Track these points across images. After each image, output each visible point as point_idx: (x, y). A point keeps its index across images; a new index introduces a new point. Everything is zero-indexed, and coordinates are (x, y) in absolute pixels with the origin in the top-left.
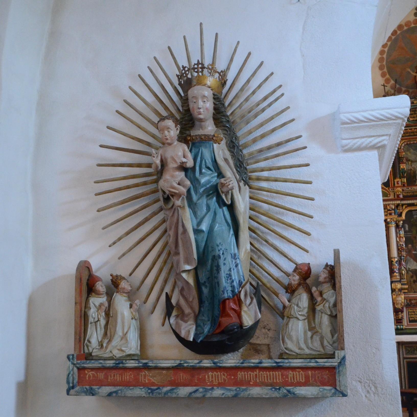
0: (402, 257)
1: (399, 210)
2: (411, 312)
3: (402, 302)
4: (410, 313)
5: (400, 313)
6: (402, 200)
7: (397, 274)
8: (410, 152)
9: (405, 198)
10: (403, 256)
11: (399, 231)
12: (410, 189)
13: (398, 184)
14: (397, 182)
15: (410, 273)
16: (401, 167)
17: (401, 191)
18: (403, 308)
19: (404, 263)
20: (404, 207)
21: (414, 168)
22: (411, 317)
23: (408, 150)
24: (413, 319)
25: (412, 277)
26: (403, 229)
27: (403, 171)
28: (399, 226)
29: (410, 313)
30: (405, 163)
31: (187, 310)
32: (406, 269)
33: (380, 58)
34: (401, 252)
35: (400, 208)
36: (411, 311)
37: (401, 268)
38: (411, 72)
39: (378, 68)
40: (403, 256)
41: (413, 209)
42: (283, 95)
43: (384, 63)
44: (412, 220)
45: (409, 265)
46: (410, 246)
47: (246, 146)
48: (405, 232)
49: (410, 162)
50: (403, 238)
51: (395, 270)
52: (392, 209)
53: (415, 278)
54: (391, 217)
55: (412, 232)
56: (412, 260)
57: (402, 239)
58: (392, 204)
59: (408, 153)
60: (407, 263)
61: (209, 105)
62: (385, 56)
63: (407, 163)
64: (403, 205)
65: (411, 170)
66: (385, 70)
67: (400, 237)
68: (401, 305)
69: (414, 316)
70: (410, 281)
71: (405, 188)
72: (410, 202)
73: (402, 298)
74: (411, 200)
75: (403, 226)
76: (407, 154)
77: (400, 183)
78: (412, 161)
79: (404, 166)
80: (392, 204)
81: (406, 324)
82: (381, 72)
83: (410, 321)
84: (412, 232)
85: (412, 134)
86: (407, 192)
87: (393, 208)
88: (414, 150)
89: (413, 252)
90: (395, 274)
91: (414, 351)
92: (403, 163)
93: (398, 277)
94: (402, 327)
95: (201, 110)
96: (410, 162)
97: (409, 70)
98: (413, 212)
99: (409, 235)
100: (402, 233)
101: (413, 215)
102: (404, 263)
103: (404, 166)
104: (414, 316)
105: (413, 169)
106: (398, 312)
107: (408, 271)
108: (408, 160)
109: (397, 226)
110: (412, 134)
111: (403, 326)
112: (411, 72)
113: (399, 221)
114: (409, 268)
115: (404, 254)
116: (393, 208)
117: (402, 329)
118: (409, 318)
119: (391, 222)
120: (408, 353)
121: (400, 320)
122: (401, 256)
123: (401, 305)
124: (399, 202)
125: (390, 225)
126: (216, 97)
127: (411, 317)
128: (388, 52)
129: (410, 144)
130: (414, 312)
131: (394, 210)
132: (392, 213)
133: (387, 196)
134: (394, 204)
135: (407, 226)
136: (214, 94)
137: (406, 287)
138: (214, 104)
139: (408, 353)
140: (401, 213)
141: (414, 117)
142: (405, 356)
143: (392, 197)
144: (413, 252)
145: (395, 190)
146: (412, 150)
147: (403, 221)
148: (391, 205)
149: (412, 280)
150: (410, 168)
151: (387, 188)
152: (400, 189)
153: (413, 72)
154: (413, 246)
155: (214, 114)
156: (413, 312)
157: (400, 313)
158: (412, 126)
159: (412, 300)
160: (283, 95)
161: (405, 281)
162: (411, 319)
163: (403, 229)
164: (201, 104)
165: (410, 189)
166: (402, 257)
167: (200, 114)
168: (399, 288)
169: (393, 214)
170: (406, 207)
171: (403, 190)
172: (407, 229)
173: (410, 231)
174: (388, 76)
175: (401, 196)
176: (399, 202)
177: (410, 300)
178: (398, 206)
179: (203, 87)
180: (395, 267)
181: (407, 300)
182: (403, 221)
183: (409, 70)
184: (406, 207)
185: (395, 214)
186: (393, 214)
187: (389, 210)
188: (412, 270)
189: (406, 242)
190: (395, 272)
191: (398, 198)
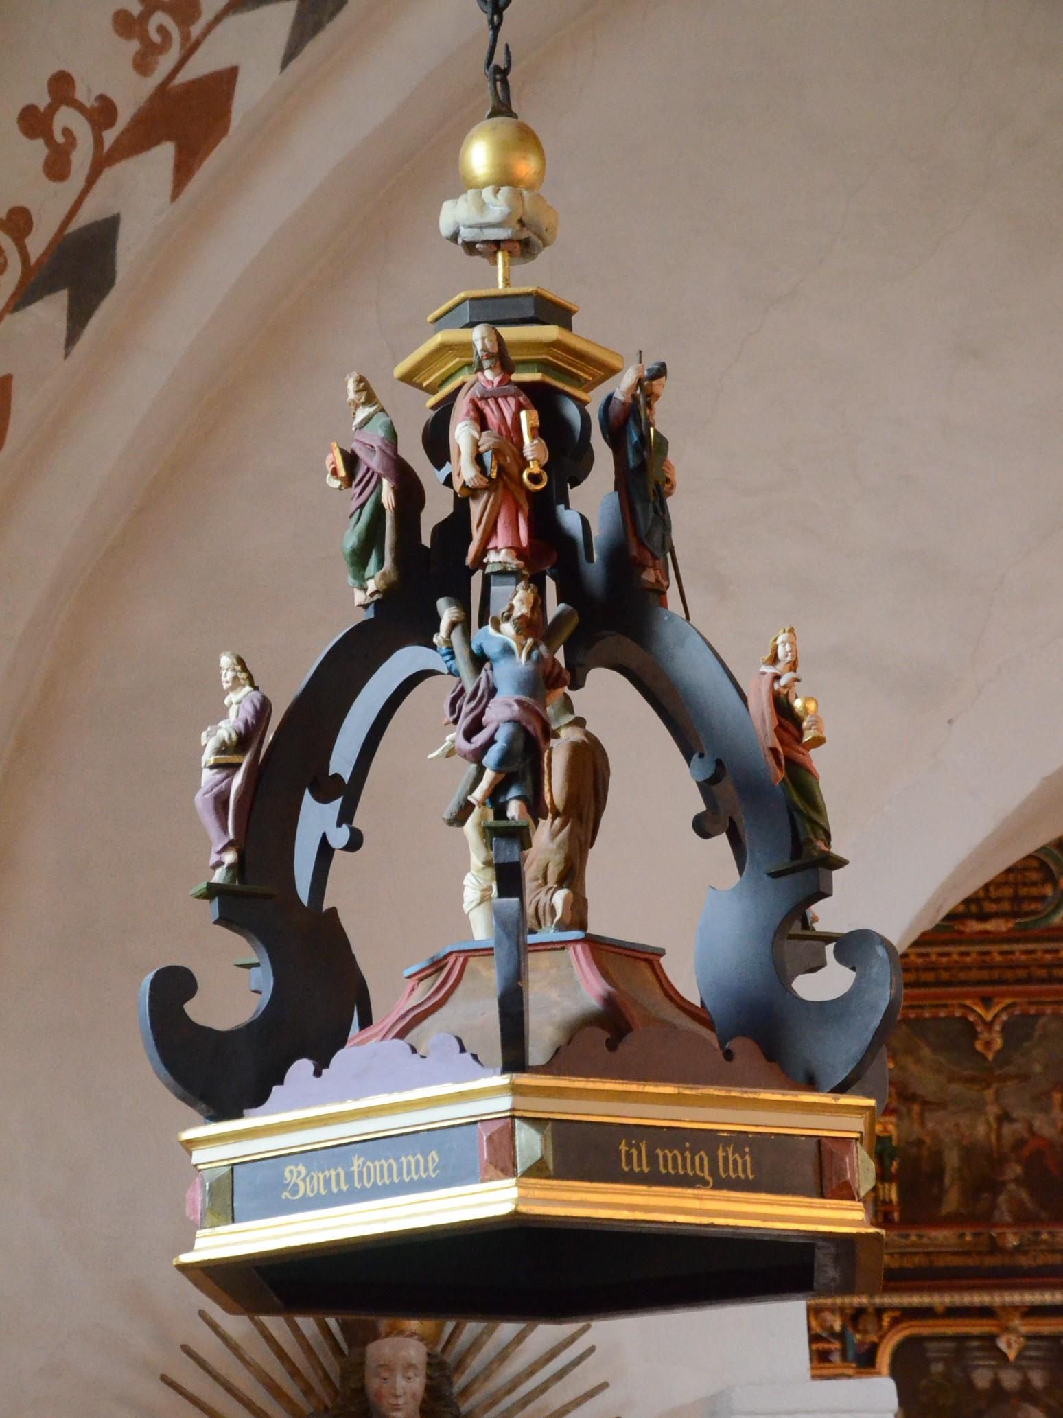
1: (865, 1332)
8: (918, 1061)
12: (913, 1238)
20: (886, 1322)
31: (166, 63)
35: (868, 1322)
42: (592, 1350)
44: (924, 1383)
47: (466, 1392)
49: (916, 1108)
52: (833, 1334)
58: (832, 1310)
59: (909, 1062)
61: (417, 1384)
63: (904, 1109)
64: (880, 1311)
65: (920, 1143)
72: (916, 1300)
74: (919, 1290)
76: (901, 1068)
78: (925, 1104)
79: (891, 1128)
80: (832, 1310)
85: (930, 977)
86: (902, 1255)
87: (837, 1327)
88: (934, 1049)
95: (401, 1401)
98: (931, 1345)
103: (891, 1128)
105: (928, 1140)
110: (930, 977)
116: (837, 1327)
126: (434, 1361)
129: (919, 1019)
131: (841, 1337)
136: (429, 1355)
138: (429, 1377)
146: (926, 1052)
150: (916, 1131)
155: (424, 1401)
160: (592, 1350)
164: (400, 1383)
165: (913, 1238)
167: (398, 1410)
169: (836, 1358)
178: (855, 1317)
179: (408, 1340)
184: (895, 1322)
185: (844, 1357)
186: (836, 1358)
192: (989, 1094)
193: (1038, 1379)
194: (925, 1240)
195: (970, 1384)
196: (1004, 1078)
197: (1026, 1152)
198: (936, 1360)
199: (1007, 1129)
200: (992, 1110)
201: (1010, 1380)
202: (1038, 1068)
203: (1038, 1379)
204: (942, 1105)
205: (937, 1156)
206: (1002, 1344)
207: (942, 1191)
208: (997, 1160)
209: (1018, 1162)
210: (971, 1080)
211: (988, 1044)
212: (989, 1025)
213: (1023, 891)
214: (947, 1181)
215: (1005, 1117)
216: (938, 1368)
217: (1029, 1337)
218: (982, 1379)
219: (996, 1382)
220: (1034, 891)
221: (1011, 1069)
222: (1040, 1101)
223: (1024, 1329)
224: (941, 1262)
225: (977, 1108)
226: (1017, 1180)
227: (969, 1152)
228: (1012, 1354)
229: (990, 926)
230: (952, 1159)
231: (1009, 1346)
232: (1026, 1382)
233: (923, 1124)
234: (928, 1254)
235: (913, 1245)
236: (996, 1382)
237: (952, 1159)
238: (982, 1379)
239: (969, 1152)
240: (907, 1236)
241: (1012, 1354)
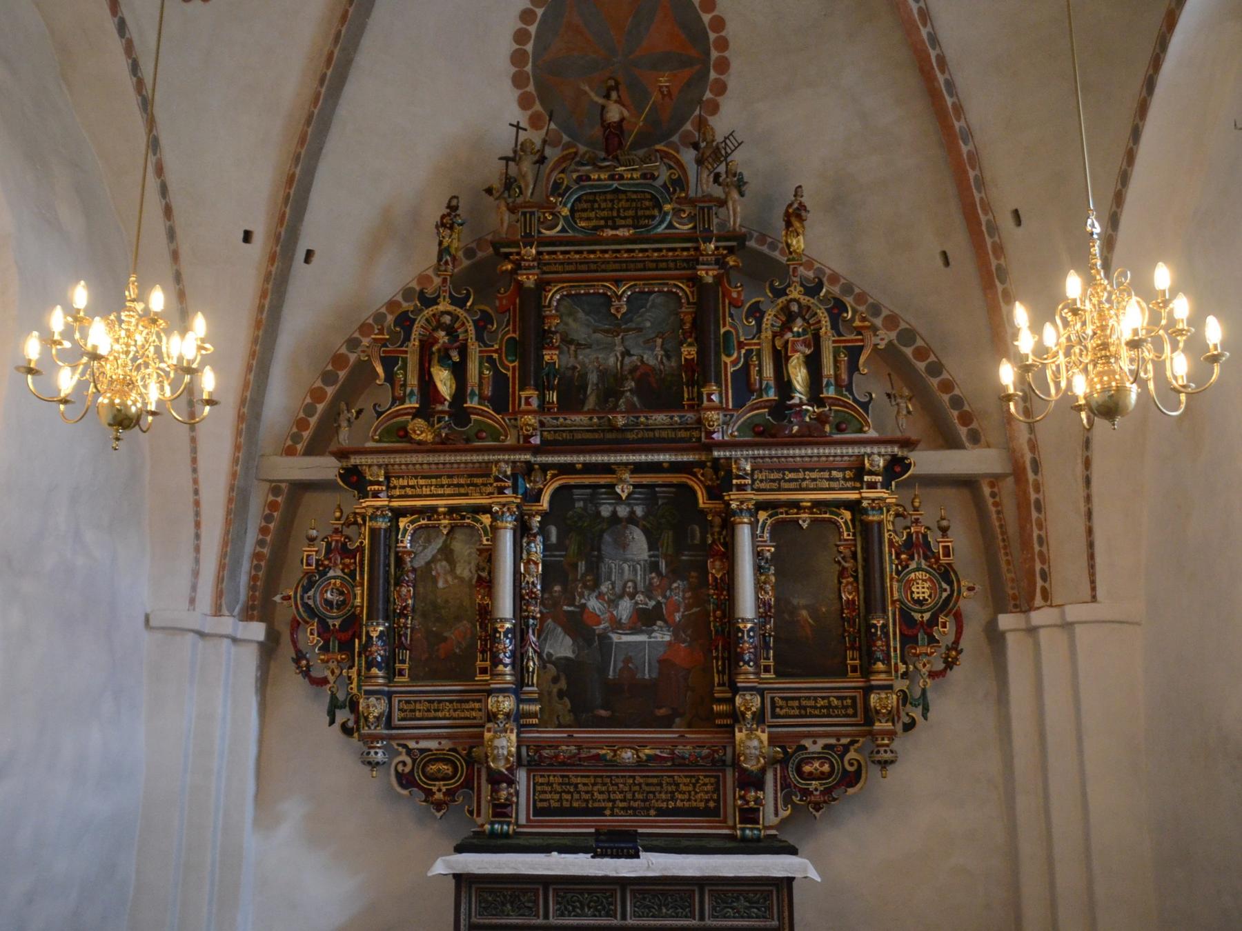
0: (531, 621)
1: (535, 482)
2: (542, 784)
3: (509, 752)
4: (539, 788)
5: (505, 785)
6: (536, 451)
7: (508, 670)
9: (547, 447)
10: (534, 618)
11: (528, 544)
12: (561, 420)
13: (528, 403)
14: (527, 398)
15: (552, 669)
16: (547, 358)
17: (537, 425)
18: (763, 771)
19: (533, 639)
21: (583, 364)
22: (541, 800)
23: (571, 314)
24: (545, 804)
25: (555, 680)
26: (539, 538)
27: (552, 370)
28: (531, 529)
29: (539, 788)
30: (558, 348)
32: (540, 655)
33: (516, 51)
34: (528, 604)
35: (537, 476)
36: (541, 780)
37: (527, 651)
38: (592, 94)
39: (510, 82)
40: (534, 618)
41: (572, 482)
43: (529, 68)
45: (551, 646)
46: (557, 588)
48: (545, 549)
49: (573, 348)
50: (536, 564)
51: (501, 656)
53: (563, 684)
54: (503, 500)
55: (566, 549)
56: (560, 629)
57: (532, 566)
58: (507, 462)
59: (570, 321)
60: (545, 639)
62: (529, 47)
64: (545, 468)
65: (574, 368)
66: (531, 88)
67: (529, 561)
68: (507, 760)
69: (548, 796)
70: (550, 693)
71: (547, 419)
73: (509, 740)
74: (565, 453)
75: (543, 530)
76: (566, 324)
77: (535, 403)
78: (579, 345)
79: (555, 357)
80: (507, 462)
81: (522, 820)
82: (517, 93)
83: (538, 812)
84: (566, 549)
85: (584, 267)
87: (509, 473)
88: (587, 314)
89: (565, 608)
90: (501, 667)
91: (504, 904)
92: (553, 348)
93: (508, 678)
94: (505, 827)
96: (573, 348)
97: (587, 88)
99: (558, 556)
100: (537, 548)
101: (573, 501)
102: (533, 639)
103: (555, 357)
104: (548, 796)
106: (499, 783)
107: (545, 661)
108: (567, 341)
109: (523, 530)
111: (509, 824)
112: (592, 94)
113: (532, 516)
114: (549, 655)
115: (535, 610)
117: (506, 835)
118: (535, 801)
119: (503, 513)
120: (485, 909)
121: (504, 806)
122: (528, 617)
123: (507, 760)
124: (528, 457)
125: (499, 524)
127: (541, 800)
128: (537, 36)
130: (551, 785)
132: (505, 488)
133: (497, 440)
134: (514, 462)
135: (553, 530)
137: (535, 708)
139: (485, 909)
140: (541, 491)
141: (588, 219)
142: (474, 920)
143: (510, 441)
144: (565, 608)
145: (519, 423)
146: (581, 315)
147: (545, 515)
148: (503, 465)
149: (555, 690)
151: (498, 417)
152: (531, 420)
153: (597, 94)
154: (565, 590)
156: (548, 784)
157: (505, 785)
158: (581, 243)
159: (544, 748)
161: (532, 690)
162: (539, 805)
163: (539, 538)
165: (561, 420)
166: (531, 621)
168: (507, 710)
170: (553, 476)
171: (542, 424)
172: (554, 539)
173: (561, 545)
174: (538, 107)
175: (536, 440)
176: (528, 457)
177: (539, 748)
180: (501, 647)
181: (528, 747)
182: (545, 515)
183: (587, 88)
184: (553, 476)
187: (497, 479)
188: (559, 659)
189: (545, 577)
190: (501, 662)
191: (526, 447)
192: (618, 340)
193: (639, 511)
194: (568, 422)
195: (599, 513)
196: (628, 330)
197: (638, 373)
198: (579, 500)
199: (627, 360)
200: (619, 349)
201: (623, 511)
202: (648, 324)
203: (639, 511)
204: (589, 346)
205: (583, 376)
206: (618, 490)
207: (586, 397)
208: (619, 379)
209: (633, 379)
210: (607, 331)
211: (618, 310)
212: (619, 298)
213: (640, 213)
214: (589, 391)
215: (626, 353)
216: (579, 504)
217: (635, 486)
218: (605, 511)
219: (614, 513)
220: (647, 213)
221: (633, 325)
222: (649, 344)
223: (632, 481)
224: (579, 436)
225: (610, 348)
226: (630, 390)
227: (603, 373)
228: (624, 496)
229: (620, 233)
230: (593, 378)
231: (623, 490)
232: (633, 512)
233: (576, 357)
234: (571, 431)
235: (561, 425)
236: (614, 513)
237: (593, 378)
238: (605, 511)
239: (603, 373)
240: (557, 419)
241: (624, 496)
